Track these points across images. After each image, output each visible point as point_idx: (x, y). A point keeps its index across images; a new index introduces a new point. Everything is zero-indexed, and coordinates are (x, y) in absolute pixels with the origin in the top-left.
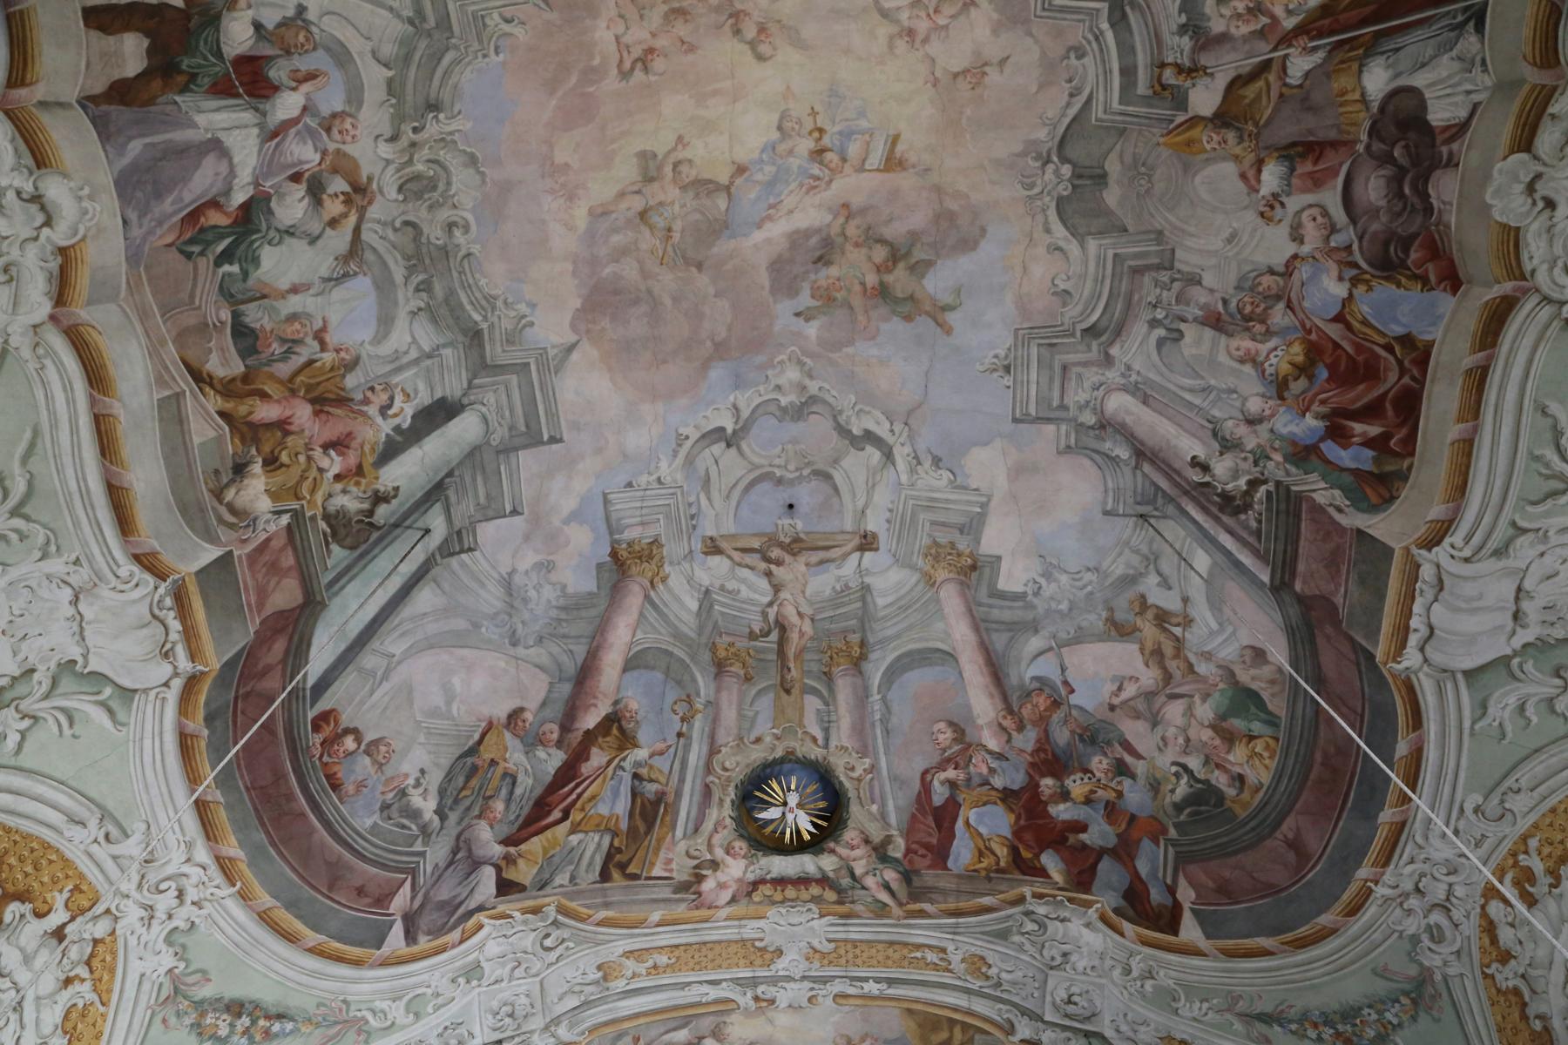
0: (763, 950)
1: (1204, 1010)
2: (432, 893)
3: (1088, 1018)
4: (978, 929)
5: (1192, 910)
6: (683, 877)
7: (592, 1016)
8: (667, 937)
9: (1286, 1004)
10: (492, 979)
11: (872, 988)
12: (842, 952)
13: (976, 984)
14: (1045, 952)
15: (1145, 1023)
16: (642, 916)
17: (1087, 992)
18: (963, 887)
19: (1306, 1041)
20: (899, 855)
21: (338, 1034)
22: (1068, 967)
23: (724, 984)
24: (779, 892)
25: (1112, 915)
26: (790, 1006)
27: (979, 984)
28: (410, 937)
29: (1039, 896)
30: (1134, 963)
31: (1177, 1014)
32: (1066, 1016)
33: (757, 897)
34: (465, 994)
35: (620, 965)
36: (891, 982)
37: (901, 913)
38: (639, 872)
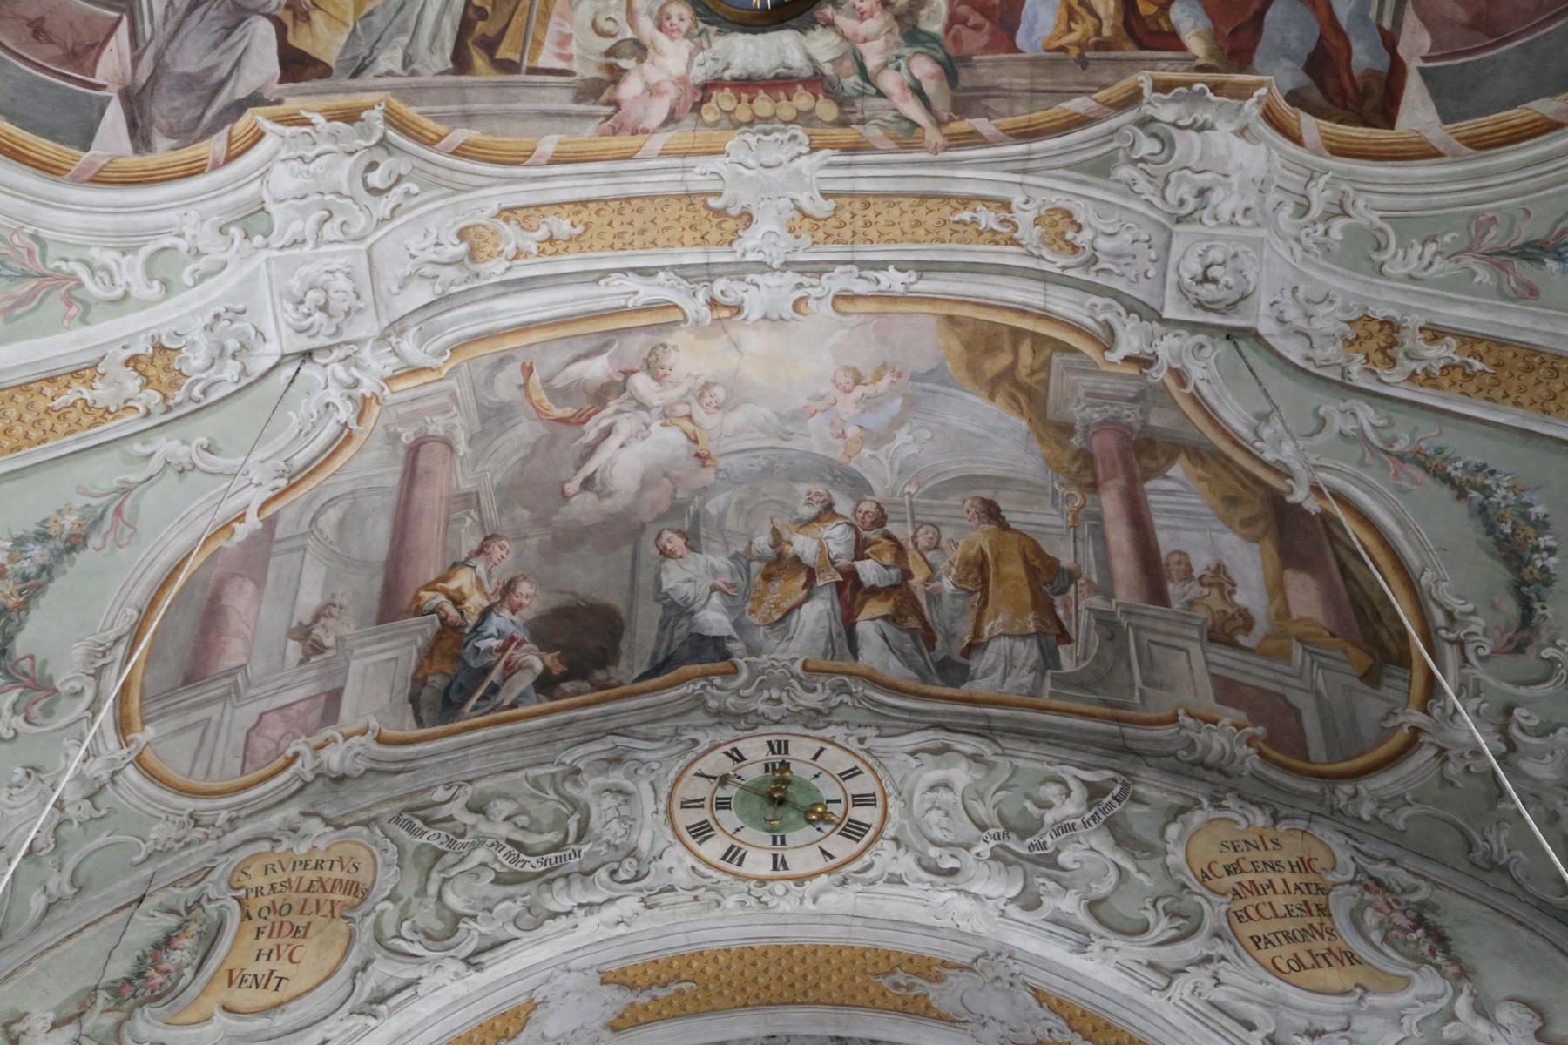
0: (720, 213)
2: (168, 58)
3: (1233, 305)
4: (1063, 161)
5: (1421, 71)
6: (587, 70)
7: (452, 324)
8: (567, 185)
10: (287, 239)
11: (892, 280)
13: (1055, 262)
14: (1169, 193)
15: (1327, 299)
16: (524, 142)
17: (1235, 256)
18: (1044, 82)
20: (936, 28)
22: (1205, 214)
23: (661, 275)
24: (745, 103)
26: (765, 317)
28: (139, 135)
29: (1163, 87)
30: (1314, 193)
31: (1380, 273)
32: (1200, 305)
33: (709, 113)
34: (245, 259)
35: (494, 233)
36: (923, 268)
37: (940, 140)
38: (516, 58)
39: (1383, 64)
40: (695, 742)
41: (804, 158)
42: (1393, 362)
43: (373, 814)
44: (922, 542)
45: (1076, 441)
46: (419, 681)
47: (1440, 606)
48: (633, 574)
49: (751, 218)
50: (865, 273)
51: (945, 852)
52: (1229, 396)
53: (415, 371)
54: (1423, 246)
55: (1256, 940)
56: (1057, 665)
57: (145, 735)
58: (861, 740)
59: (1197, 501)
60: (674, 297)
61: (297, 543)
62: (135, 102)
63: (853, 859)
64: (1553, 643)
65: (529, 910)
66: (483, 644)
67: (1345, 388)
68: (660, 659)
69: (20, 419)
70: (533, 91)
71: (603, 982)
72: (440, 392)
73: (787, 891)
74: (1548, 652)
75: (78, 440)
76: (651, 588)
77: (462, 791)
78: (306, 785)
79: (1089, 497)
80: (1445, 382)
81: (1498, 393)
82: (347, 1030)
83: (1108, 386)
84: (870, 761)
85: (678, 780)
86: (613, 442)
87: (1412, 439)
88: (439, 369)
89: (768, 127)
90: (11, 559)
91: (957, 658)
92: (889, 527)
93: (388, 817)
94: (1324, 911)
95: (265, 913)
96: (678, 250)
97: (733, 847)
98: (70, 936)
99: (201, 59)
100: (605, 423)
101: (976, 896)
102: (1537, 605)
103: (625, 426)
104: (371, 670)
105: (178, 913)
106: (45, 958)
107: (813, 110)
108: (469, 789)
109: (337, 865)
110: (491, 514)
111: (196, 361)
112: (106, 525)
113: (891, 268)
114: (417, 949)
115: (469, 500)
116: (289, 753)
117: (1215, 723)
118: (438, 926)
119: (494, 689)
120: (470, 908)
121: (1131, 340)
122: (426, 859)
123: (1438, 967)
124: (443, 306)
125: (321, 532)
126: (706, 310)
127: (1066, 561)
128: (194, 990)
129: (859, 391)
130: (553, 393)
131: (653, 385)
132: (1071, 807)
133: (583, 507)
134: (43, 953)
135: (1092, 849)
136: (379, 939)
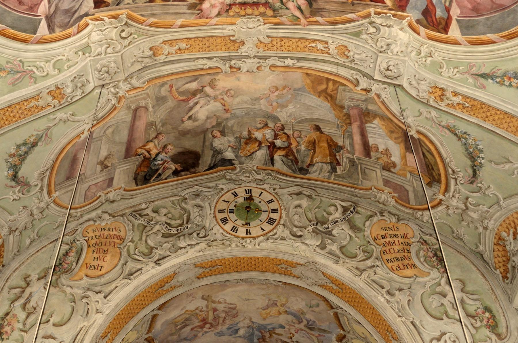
1: (455, 73)
2: (59, 5)
4: (345, 32)
5: (457, 20)
8: (185, 34)
9: (497, 68)
10: (96, 53)
12: (275, 43)
13: (342, 60)
14: (378, 44)
15: (424, 80)
17: (397, 64)
18: (340, 8)
19: (503, 87)
21: (18, 79)
22: (389, 51)
23: (215, 59)
25: (415, 23)
26: (248, 71)
27: (343, 60)
28: (51, 28)
29: (379, 14)
33: (231, 13)
34: (83, 60)
36: (299, 59)
37: (306, 23)
39: (446, 16)
40: (222, 189)
41: (261, 26)
42: (443, 100)
43: (124, 213)
44: (296, 135)
45: (345, 111)
46: (137, 174)
47: (451, 168)
48: (204, 142)
49: (244, 43)
50: (280, 60)
51: (299, 229)
52: (393, 103)
53: (136, 88)
54: (454, 69)
55: (388, 260)
56: (336, 171)
57: (55, 195)
58: (274, 190)
59: (382, 131)
60: (218, 65)
61: (100, 138)
62: (49, 19)
63: (270, 231)
64: (481, 183)
65: (173, 246)
66: (156, 163)
67: (427, 104)
68: (212, 165)
69: (18, 112)
70: (174, 7)
71: (195, 267)
72: (144, 94)
73: (251, 242)
74: (479, 185)
75: (34, 116)
76: (210, 147)
77: (150, 205)
78: (103, 204)
79: (348, 126)
80: (457, 108)
81: (472, 113)
82: (123, 284)
83: (356, 96)
84: (277, 197)
85: (217, 202)
86: (198, 106)
87: (447, 122)
88: (143, 87)
89: (250, 17)
90: (17, 152)
91: (305, 167)
92: (285, 131)
93: (128, 214)
94: (409, 251)
95: (94, 245)
96: (220, 52)
97: (234, 226)
98: (38, 251)
99: (69, 4)
100: (196, 101)
101: (307, 244)
102: (478, 172)
103: (202, 102)
104: (122, 172)
105: (69, 244)
106: (32, 258)
107: (265, 12)
108: (153, 204)
109: (114, 229)
110: (159, 127)
111: (69, 90)
112: (43, 139)
113: (289, 59)
114: (140, 258)
115: (152, 124)
116: (98, 196)
117: (383, 191)
118: (146, 251)
119: (160, 175)
120: (156, 245)
121: (364, 83)
122: (141, 228)
123: (438, 269)
124: (145, 69)
125: (107, 135)
126: (229, 69)
127: (340, 144)
128: (77, 270)
129: (276, 93)
130: (180, 93)
131: (212, 90)
132: (337, 215)
133: (189, 124)
134: (31, 256)
135: (343, 229)
136: (129, 255)
